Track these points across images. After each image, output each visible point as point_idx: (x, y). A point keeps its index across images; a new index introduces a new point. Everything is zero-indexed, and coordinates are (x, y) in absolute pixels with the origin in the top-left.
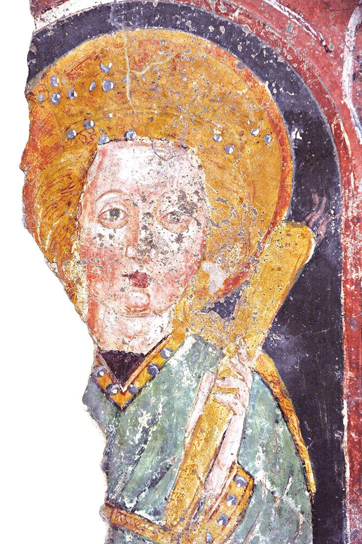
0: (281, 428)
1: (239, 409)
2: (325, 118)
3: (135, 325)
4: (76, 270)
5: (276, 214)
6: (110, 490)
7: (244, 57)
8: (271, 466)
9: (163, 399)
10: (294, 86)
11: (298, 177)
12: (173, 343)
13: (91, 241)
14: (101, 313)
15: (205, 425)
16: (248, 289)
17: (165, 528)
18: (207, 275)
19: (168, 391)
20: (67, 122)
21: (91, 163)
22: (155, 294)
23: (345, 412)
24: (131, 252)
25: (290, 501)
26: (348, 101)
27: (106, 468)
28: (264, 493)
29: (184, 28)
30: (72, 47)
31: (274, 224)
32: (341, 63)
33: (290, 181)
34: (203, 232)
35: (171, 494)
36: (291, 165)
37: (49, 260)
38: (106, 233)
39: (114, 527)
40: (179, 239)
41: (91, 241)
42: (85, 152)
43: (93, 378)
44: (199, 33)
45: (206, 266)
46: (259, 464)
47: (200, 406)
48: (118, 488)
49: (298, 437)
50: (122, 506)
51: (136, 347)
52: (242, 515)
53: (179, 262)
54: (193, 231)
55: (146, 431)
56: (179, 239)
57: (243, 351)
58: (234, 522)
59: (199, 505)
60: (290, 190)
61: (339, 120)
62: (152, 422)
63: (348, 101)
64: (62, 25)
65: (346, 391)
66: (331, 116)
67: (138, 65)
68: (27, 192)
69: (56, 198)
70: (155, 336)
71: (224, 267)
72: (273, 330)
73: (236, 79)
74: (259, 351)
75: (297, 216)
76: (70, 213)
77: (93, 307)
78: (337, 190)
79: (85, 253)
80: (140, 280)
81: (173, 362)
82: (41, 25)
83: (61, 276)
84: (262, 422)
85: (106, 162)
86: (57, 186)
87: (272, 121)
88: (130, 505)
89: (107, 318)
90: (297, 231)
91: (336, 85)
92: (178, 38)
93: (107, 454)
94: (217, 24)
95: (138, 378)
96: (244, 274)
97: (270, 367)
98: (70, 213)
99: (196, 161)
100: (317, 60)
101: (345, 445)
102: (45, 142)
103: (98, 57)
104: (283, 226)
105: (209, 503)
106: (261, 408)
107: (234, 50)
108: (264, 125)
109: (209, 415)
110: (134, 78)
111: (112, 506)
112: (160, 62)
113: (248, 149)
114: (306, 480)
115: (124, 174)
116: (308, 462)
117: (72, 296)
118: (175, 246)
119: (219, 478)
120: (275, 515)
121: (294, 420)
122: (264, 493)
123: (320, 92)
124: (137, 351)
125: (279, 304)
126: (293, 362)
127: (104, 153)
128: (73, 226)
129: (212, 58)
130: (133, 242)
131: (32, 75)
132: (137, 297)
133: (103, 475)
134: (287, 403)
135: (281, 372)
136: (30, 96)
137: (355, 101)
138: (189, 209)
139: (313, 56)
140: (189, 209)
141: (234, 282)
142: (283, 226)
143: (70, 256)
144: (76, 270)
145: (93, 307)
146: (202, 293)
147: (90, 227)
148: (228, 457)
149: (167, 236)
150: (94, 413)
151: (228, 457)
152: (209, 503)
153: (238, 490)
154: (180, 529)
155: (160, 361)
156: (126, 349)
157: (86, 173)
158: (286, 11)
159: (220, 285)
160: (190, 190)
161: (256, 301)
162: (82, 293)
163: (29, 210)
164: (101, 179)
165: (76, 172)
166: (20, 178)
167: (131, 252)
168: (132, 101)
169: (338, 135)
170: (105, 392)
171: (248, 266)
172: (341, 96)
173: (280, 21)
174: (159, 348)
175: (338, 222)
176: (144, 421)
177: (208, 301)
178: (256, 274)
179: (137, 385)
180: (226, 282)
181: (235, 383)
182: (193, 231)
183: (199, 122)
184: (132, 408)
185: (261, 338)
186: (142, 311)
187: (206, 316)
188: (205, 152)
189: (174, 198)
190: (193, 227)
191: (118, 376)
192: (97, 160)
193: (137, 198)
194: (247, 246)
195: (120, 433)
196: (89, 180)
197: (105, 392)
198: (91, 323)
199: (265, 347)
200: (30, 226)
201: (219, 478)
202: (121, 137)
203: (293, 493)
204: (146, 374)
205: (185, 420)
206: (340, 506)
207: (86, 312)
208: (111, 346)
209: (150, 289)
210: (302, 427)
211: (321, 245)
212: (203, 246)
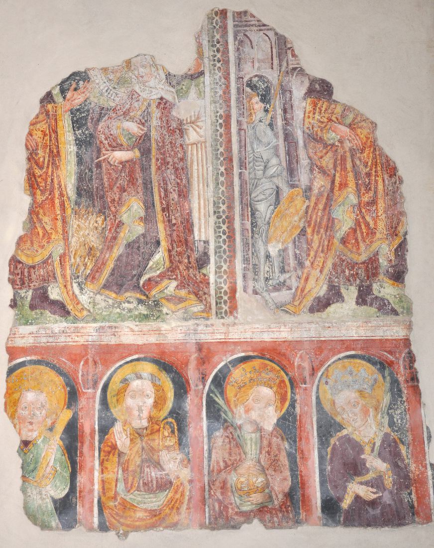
0: (63, 457)
1: (54, 453)
2: (75, 385)
3: (30, 434)
4: (16, 421)
5: (64, 407)
6: (23, 473)
7: (57, 371)
8: (61, 466)
9: (36, 451)
10: (68, 378)
11: (69, 399)
12: (39, 438)
13: (20, 414)
14: (22, 432)
15: (45, 457)
16: (57, 425)
17: (35, 481)
18: (47, 422)
19: (37, 449)
20: (15, 387)
21: (20, 396)
22: (35, 427)
23: (78, 453)
24: (29, 417)
25: (65, 474)
26: (80, 381)
27: (22, 468)
28: (59, 472)
29: (43, 365)
30: (17, 370)
31: (63, 409)
32: (79, 373)
33: (67, 399)
34: (280, 383)
35: (212, 67)
36: (67, 396)
37: (10, 419)
38: (23, 412)
39: (24, 481)
40: (41, 413)
41: (20, 414)
42: (19, 394)
43: (19, 447)
44: (47, 366)
45: (47, 419)
46: (58, 466)
47: (44, 452)
48: (24, 473)
49: (67, 459)
50: (26, 476)
51: (29, 439)
52: (54, 477)
53: (40, 419)
54: (44, 412)
55: (31, 459)
56: (41, 413)
57: (55, 439)
58: (52, 479)
59: (43, 476)
60: (67, 402)
61: (78, 385)
62: (33, 457)
63: (80, 381)
64: (15, 365)
65: (79, 448)
66: (76, 385)
67: (32, 374)
68: (6, 404)
69: (12, 404)
70: (34, 436)
71: (51, 420)
72: (62, 434)
73: (55, 376)
74: (59, 439)
75: (68, 408)
76: (15, 408)
77: (20, 430)
78: (78, 401)
79: (18, 417)
80: (31, 423)
81: (38, 442)
82: (10, 366)
83: (13, 423)
84: (59, 456)
85: (24, 396)
86: (12, 402)
87: (63, 386)
88: (27, 476)
89: (23, 433)
90: (68, 411)
91: (78, 378)
92: (42, 367)
93: (23, 464)
94: (51, 364)
95: (30, 447)
96: (56, 421)
97: (61, 443)
98: (15, 408)
99: (45, 395)
100: (73, 372)
101: (78, 461)
102: (10, 391)
103: (23, 372)
104: (65, 410)
105: (46, 475)
106: (59, 453)
107: (55, 370)
108: (61, 387)
109: (47, 454)
110: (31, 376)
111: (23, 476)
112: (37, 373)
113: (57, 392)
114: (69, 469)
115: (28, 399)
116: (69, 465)
117: (15, 427)
118: (39, 415)
119: (49, 469)
120: (73, 236)
121: (67, 455)
122: (59, 472)
123: (74, 379)
124: (30, 440)
125: (64, 428)
126: (67, 442)
127: (23, 394)
128: (16, 411)
129: (49, 372)
130: (30, 414)
131: (7, 377)
132: (30, 427)
133: (21, 469)
134: (65, 451)
135: (64, 444)
136: (7, 381)
137: (82, 381)
138: (43, 406)
139: (72, 371)
140: (43, 406)
141: (53, 423)
142: (65, 410)
143: (15, 418)
144: (16, 421)
145: (20, 430)
146: (45, 426)
147: (20, 411)
148: (51, 464)
149: (38, 413)
150: (20, 455)
151: (51, 464)
152: (46, 475)
153: (53, 472)
154: (39, 481)
155: (35, 442)
156: (28, 440)
157: (19, 398)
158: (66, 361)
159: (50, 424)
160: (43, 402)
161: (58, 427)
162: (17, 427)
163: (6, 407)
164: (23, 400)
165: (17, 398)
166: (4, 400)
167: (29, 417)
168: (31, 382)
169: (78, 389)
170: (22, 450)
171: (57, 419)
172: (79, 380)
173: (65, 364)
174: (35, 439)
175: (78, 409)
176: (31, 457)
177: (47, 428)
178: (58, 421)
179: (30, 448)
180: (51, 423)
181: (53, 447)
182: (44, 412)
183: (46, 386)
184: (28, 454)
185: (60, 436)
186: (32, 430)
187: (47, 431)
188: (48, 393)
189: (40, 404)
190: (44, 411)
191: (25, 446)
192: (22, 396)
193: (31, 404)
194: (57, 415)
195: (26, 459)
196: (20, 400)
197: (22, 450)
198: (19, 433)
199: (60, 438)
200: (6, 411)
201: (49, 469)
202: (28, 390)
203: (65, 472)
204: (32, 445)
205: (41, 456)
206: (76, 475)
207: (18, 430)
208: (24, 439)
209: (34, 425)
210: (68, 456)
211: (74, 414)
212: (46, 415)
